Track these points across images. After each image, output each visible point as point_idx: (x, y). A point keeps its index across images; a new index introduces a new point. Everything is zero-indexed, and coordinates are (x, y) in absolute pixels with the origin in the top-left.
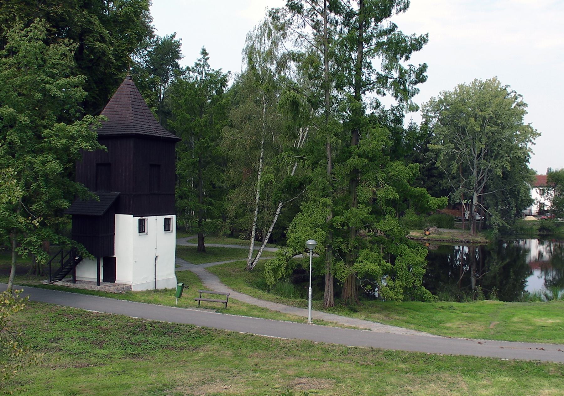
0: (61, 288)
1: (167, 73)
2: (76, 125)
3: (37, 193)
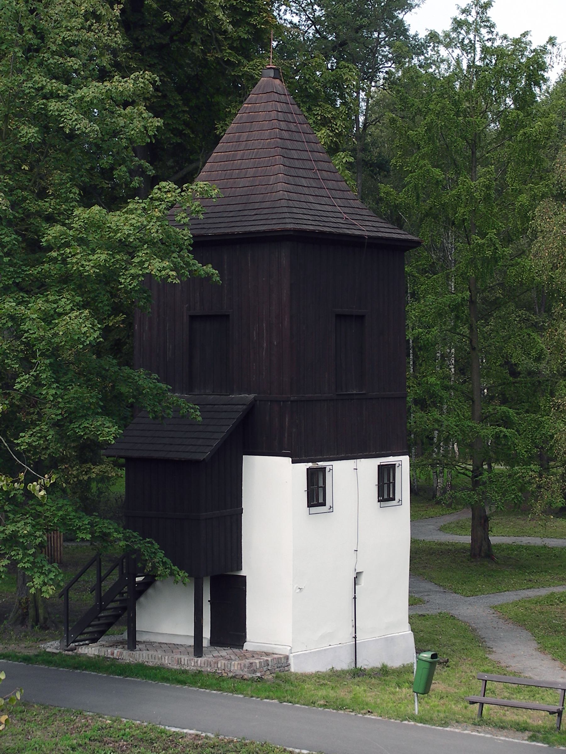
0: (95, 665)
1: (374, 52)
2: (131, 212)
3: (31, 399)
